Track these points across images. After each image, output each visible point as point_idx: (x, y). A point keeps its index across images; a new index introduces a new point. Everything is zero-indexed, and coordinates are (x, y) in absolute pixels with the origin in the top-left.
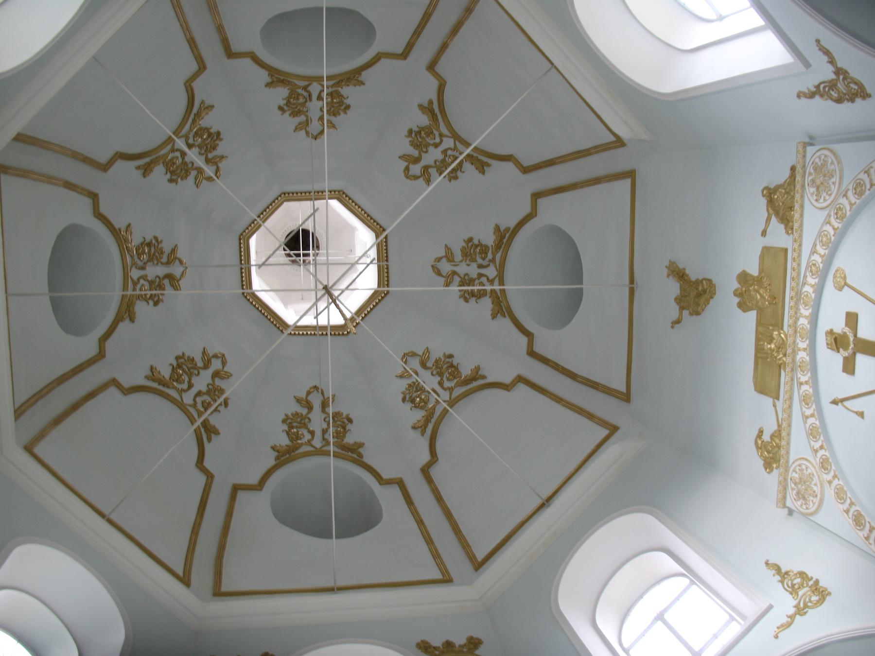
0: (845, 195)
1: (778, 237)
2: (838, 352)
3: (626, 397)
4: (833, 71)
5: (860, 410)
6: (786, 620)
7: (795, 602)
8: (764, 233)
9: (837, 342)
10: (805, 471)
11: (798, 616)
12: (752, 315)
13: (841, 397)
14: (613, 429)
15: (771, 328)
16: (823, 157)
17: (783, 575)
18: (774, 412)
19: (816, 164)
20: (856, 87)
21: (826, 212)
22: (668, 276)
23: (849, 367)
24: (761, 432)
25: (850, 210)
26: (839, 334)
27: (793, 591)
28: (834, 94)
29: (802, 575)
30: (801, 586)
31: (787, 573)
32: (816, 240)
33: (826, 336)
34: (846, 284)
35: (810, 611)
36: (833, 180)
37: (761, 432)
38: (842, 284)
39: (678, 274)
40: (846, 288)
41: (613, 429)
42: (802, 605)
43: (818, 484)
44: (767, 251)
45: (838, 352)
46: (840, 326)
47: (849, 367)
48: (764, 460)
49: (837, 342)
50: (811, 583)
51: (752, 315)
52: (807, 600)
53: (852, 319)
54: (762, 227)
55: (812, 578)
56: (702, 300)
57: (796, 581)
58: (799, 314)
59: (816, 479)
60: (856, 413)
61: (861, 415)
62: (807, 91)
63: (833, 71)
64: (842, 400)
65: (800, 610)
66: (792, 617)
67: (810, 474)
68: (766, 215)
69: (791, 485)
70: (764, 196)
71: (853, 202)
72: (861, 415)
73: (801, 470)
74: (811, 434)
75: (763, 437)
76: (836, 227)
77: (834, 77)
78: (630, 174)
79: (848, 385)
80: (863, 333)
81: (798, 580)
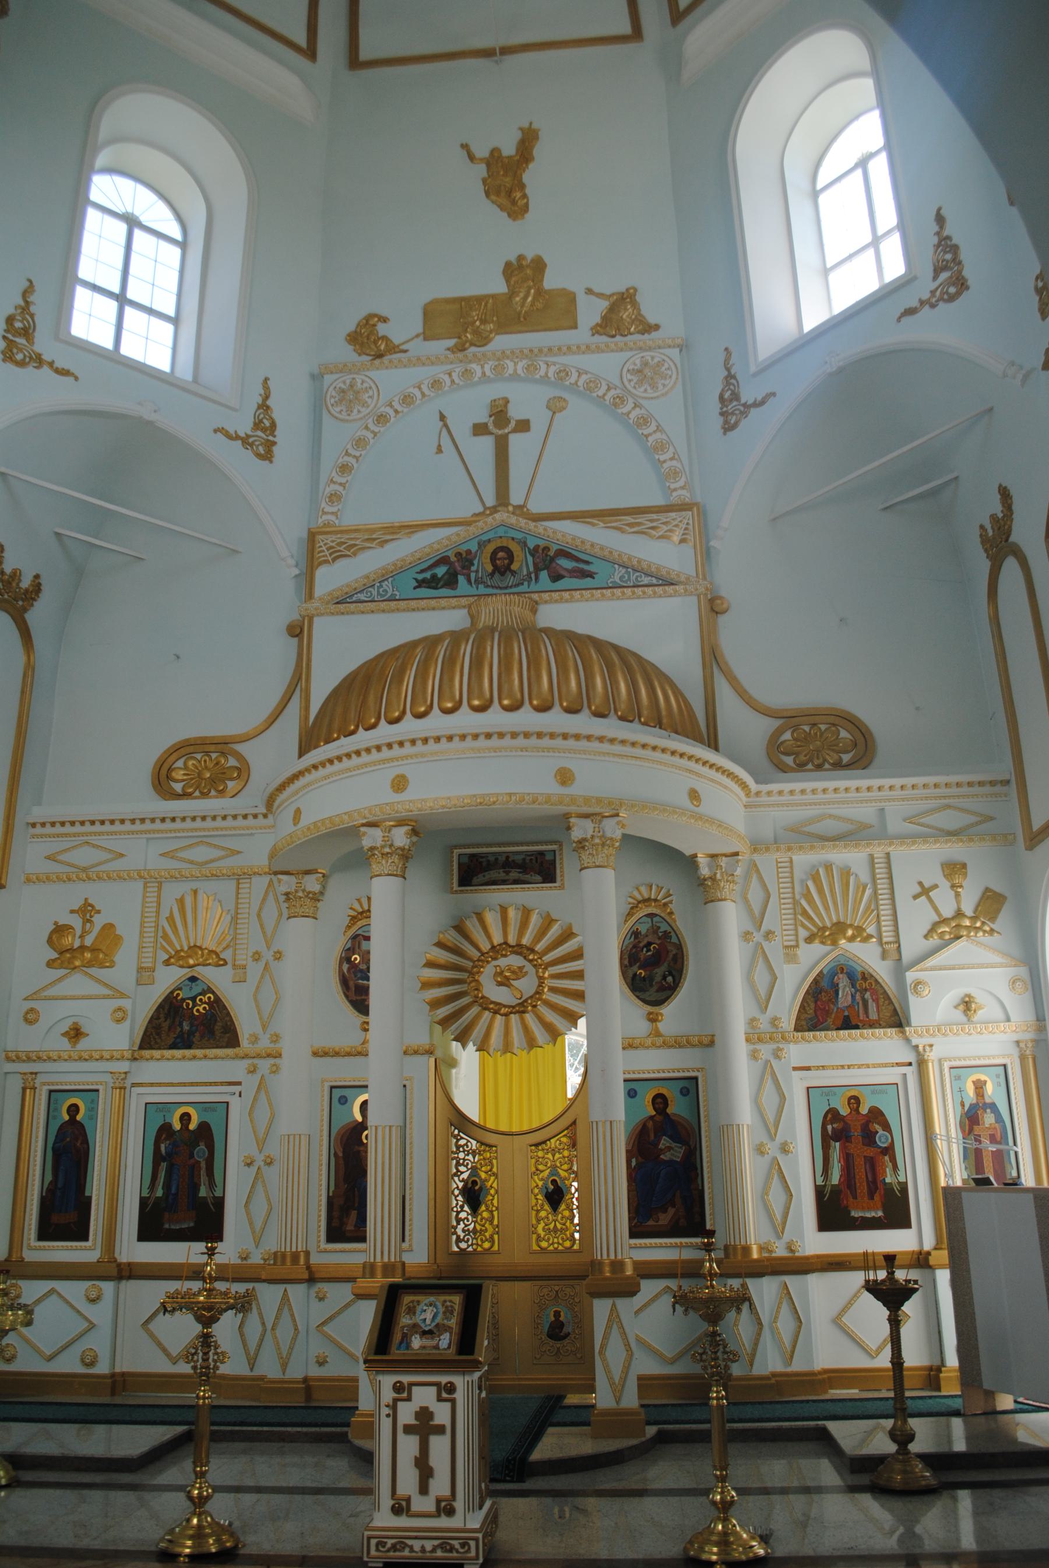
0: (636, 406)
1: (590, 311)
2: (491, 416)
3: (355, 62)
4: (416, 1457)
5: (443, 449)
6: (232, 432)
7: (249, 433)
8: (589, 291)
9: (500, 413)
10: (367, 395)
11: (240, 442)
12: (500, 287)
13: (448, 422)
14: (310, 52)
15: (495, 319)
16: (669, 372)
17: (264, 407)
18: (410, 337)
19: (663, 365)
20: (732, 422)
21: (617, 383)
22: (521, 129)
23: (479, 430)
24: (385, 320)
25: (622, 413)
26: (507, 413)
27: (257, 425)
28: (727, 395)
29: (273, 425)
30: (264, 430)
31: (268, 407)
32: (592, 374)
33: (503, 398)
34: (554, 413)
35: (249, 452)
36: (649, 390)
37: (385, 320)
38: (555, 406)
39: (528, 140)
40: (551, 413)
41: (310, 52)
42: (251, 440)
43: (361, 415)
44: (571, 298)
45: (491, 416)
46: (515, 413)
47: (479, 430)
48: (356, 332)
49: (500, 413)
50: (271, 438)
51: (500, 287)
52: (257, 443)
53: (524, 426)
54: (597, 290)
55: (275, 436)
56: (503, 200)
57: (265, 421)
58: (516, 360)
59: (365, 411)
60: (439, 446)
61: (439, 450)
62: (731, 363)
63: (416, 1457)
64: (446, 426)
65: (246, 441)
66: (237, 437)
67: (366, 402)
68: (608, 293)
69: (348, 379)
70: (627, 290)
71: (630, 416)
72: (439, 450)
73: (366, 390)
74: (405, 396)
75: (380, 323)
76: (606, 398)
77: (743, 401)
78: (637, 33)
79: (462, 430)
80: (512, 438)
81: (267, 423)
